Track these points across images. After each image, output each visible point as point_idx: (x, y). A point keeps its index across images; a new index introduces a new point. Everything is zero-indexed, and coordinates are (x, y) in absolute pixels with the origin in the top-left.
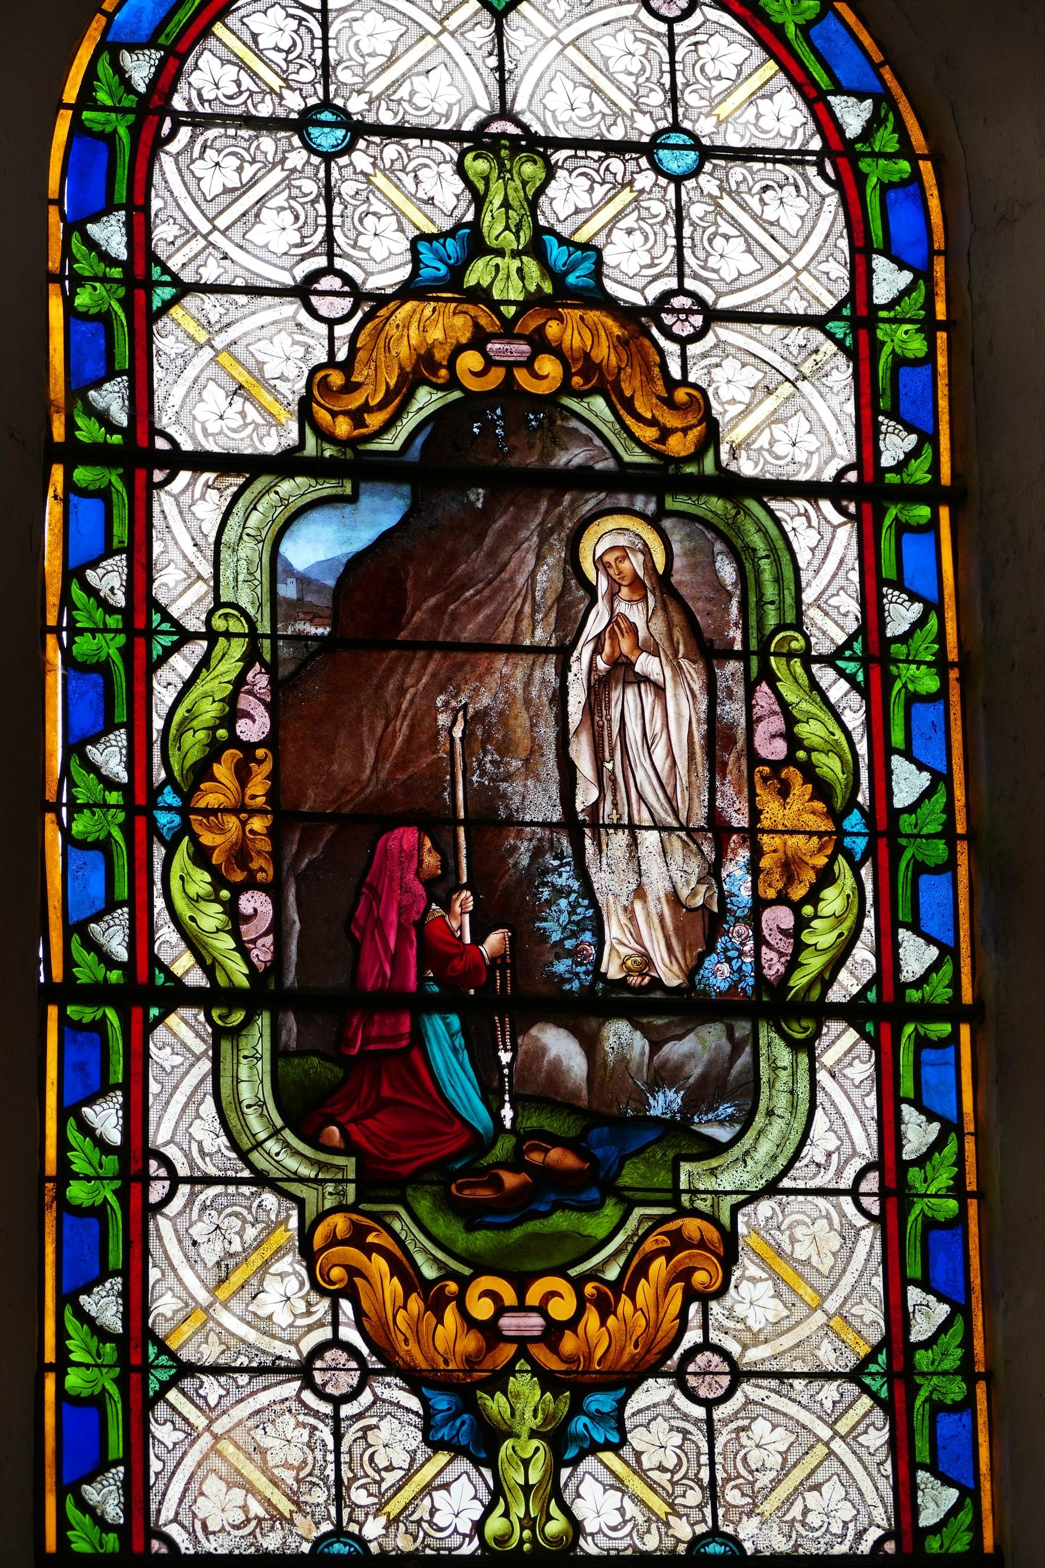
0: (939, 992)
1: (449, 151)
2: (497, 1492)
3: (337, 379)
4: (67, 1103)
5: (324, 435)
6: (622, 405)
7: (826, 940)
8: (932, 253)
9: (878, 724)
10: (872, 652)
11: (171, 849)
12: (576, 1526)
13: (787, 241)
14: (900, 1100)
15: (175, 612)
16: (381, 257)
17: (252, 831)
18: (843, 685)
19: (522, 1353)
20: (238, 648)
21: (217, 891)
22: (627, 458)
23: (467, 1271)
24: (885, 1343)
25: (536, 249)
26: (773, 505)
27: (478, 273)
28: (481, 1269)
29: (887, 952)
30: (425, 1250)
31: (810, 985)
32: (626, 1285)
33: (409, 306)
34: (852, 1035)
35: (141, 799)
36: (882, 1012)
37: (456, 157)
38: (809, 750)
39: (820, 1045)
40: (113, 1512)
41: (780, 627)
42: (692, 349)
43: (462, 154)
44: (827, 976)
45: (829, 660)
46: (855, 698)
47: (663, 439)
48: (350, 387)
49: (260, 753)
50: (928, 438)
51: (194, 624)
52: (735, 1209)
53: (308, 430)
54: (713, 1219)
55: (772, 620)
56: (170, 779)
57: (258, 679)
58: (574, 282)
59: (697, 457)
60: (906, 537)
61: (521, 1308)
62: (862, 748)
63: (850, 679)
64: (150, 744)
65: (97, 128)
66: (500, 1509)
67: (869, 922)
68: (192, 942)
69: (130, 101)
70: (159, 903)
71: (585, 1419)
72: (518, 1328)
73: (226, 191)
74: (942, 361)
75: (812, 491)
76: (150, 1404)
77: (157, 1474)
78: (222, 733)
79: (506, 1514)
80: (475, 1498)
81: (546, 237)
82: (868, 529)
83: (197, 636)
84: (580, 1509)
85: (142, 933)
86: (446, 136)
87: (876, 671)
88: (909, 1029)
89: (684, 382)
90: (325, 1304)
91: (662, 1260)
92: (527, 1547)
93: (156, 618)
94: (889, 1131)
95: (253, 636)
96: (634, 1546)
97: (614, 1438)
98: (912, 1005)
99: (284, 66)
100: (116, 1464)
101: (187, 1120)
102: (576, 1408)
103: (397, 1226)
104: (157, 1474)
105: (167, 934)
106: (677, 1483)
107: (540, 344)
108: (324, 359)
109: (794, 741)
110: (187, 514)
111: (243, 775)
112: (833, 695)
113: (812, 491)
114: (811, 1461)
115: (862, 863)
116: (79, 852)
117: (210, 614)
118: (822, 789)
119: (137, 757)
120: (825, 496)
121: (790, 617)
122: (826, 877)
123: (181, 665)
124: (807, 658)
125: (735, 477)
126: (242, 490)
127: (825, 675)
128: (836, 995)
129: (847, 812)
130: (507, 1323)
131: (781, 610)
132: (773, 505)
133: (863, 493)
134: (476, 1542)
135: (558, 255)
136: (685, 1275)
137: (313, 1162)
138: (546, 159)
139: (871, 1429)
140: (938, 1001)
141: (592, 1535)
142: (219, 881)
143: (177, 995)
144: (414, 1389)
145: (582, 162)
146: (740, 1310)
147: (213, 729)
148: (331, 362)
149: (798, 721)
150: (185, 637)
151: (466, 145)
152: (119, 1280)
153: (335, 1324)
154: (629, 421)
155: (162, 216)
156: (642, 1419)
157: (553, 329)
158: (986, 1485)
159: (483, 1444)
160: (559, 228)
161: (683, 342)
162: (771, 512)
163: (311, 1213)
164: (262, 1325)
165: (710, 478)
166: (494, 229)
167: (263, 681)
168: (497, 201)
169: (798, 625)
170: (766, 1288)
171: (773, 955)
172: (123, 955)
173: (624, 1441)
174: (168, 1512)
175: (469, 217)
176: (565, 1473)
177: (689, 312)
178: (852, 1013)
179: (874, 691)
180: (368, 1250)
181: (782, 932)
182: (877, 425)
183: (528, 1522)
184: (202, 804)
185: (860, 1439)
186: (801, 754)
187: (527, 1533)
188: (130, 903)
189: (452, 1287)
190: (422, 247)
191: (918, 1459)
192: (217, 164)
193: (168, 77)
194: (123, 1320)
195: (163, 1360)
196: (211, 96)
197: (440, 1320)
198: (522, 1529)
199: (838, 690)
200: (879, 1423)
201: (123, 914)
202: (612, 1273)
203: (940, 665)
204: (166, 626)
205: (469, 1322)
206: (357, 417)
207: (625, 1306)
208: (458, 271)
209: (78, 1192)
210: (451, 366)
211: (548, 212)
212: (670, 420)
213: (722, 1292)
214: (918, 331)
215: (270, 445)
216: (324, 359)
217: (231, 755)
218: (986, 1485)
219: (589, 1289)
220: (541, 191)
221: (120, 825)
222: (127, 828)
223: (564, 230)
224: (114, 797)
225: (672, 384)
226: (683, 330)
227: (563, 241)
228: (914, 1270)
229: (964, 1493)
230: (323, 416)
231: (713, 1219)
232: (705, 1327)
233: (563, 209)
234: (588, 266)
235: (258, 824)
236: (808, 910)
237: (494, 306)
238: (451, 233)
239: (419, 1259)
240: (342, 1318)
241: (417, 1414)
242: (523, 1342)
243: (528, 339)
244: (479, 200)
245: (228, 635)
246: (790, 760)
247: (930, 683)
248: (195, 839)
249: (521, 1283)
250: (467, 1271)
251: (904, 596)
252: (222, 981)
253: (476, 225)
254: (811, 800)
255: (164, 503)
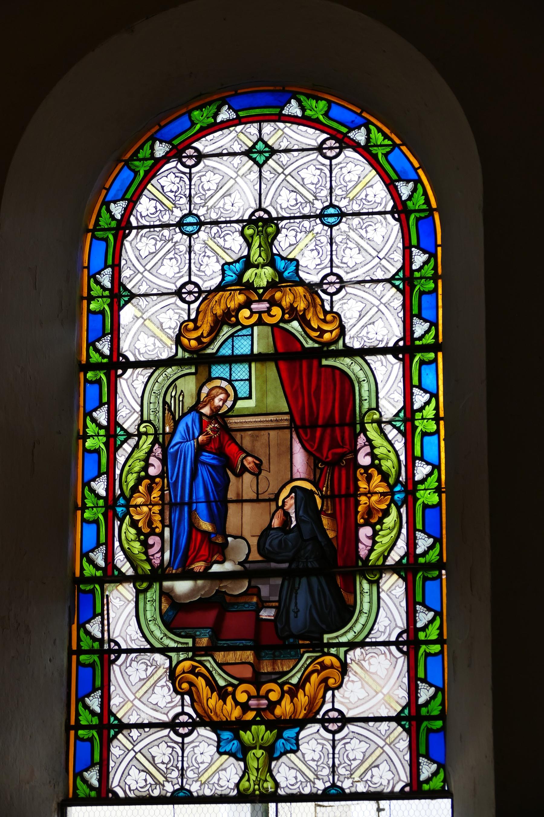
0: (429, 340)
1: (238, 227)
2: (246, 771)
3: (191, 325)
4: (77, 771)
5: (185, 349)
6: (305, 322)
7: (386, 540)
8: (437, 246)
9: (414, 746)
10: (409, 413)
11: (122, 521)
12: (277, 785)
13: (375, 244)
14: (416, 530)
15: (125, 426)
16: (210, 276)
17: (153, 513)
18: (395, 432)
19: (260, 296)
20: (151, 438)
21: (139, 537)
22: (306, 346)
23: (236, 682)
24: (408, 705)
25: (272, 263)
26: (367, 358)
27: (249, 275)
28: (242, 681)
29: (412, 543)
30: (220, 675)
31: (378, 559)
32: (301, 685)
33: (221, 293)
34: (395, 577)
35: (110, 503)
36: (408, 569)
37: (240, 229)
38: (380, 460)
39: (382, 582)
40: (95, 782)
41: (370, 409)
42: (335, 298)
43: (243, 228)
44: (386, 554)
45: (389, 422)
46: (400, 437)
47: (321, 336)
48: (196, 328)
49: (157, 480)
50: (433, 255)
51: (132, 430)
52: (346, 653)
53: (179, 348)
54: (337, 656)
55: (366, 406)
56: (122, 494)
57: (158, 450)
58: (287, 277)
59: (335, 341)
60: (427, 511)
61: (260, 313)
62: (402, 458)
63: (398, 429)
64: (115, 480)
65: (87, 662)
66: (246, 778)
67: (404, 531)
68: (129, 557)
69: (114, 224)
70: (117, 544)
71: (283, 741)
72: (257, 308)
73: (150, 253)
74: (440, 291)
75: (384, 351)
76: (110, 740)
77: (112, 767)
78: (143, 474)
79: (248, 780)
80: (236, 774)
81: (275, 257)
82: (405, 224)
83: (135, 435)
84: (278, 778)
85: (109, 557)
86: (237, 222)
87: (409, 424)
88: (420, 574)
89: (331, 312)
90: (179, 697)
91: (315, 675)
92: (257, 792)
93: (118, 429)
94: (414, 769)
95: (156, 434)
96: (300, 792)
97: (295, 748)
98: (422, 564)
99: (174, 198)
100: (108, 334)
101: (125, 626)
102: (279, 736)
103: (208, 665)
104: (112, 767)
105: (120, 556)
106: (317, 188)
107: (273, 302)
108: (186, 318)
109: (374, 456)
110: (131, 387)
111: (150, 490)
112: (390, 437)
113: (384, 351)
114: (374, 686)
115: (401, 506)
116: (83, 668)
117: (139, 425)
118: (385, 476)
119: (110, 488)
120: (389, 353)
121: (374, 405)
122: (386, 513)
123: (127, 447)
124: (379, 422)
125: (352, 349)
126: (152, 374)
127: (388, 428)
128: (390, 562)
129: (395, 485)
130: (252, 702)
131: (370, 403)
132: (367, 358)
133: (405, 350)
134: (236, 792)
135: (281, 264)
136: (325, 680)
137: (175, 642)
138: (277, 225)
139: (401, 741)
140: (433, 561)
141: (283, 788)
142: (139, 532)
143: (122, 579)
144: (214, 730)
145: (292, 224)
146: (347, 695)
147: (139, 473)
148: (189, 320)
149: (375, 448)
150: (129, 436)
151: (245, 224)
152: (105, 476)
153: (183, 705)
154: (307, 330)
155: (125, 267)
156: (304, 740)
157: (278, 295)
158: (444, 536)
159: (242, 753)
160: (282, 253)
161: (332, 295)
162: (366, 361)
163: (174, 663)
164: (154, 707)
165: (341, 350)
166: (255, 257)
167: (159, 451)
168: (257, 244)
169: (377, 408)
170: (358, 684)
171: (364, 546)
172: (98, 710)
173: (298, 749)
174: (115, 783)
175: (246, 253)
176: (274, 763)
177: (334, 283)
178: (396, 569)
179: (408, 433)
180: (197, 675)
181: (368, 537)
182: (417, 686)
183: (258, 782)
184: (134, 503)
185: (396, 745)
186: (377, 462)
187: (257, 787)
188: (106, 544)
189: (230, 689)
190: (226, 267)
191: (413, 244)
192: (148, 210)
193: (128, 211)
194: (110, 350)
195: (122, 433)
196: (135, 638)
197: (225, 703)
198: (255, 785)
199: (392, 433)
200: (405, 738)
201: (104, 477)
202: (295, 681)
203: (437, 419)
204: (122, 433)
205: (237, 703)
206: (198, 339)
207: (301, 694)
208: (241, 275)
209: (90, 443)
210: (237, 317)
211: (278, 247)
212: (325, 327)
213: (340, 686)
214: (434, 492)
215: (164, 356)
216: (186, 318)
217: (146, 482)
218: (444, 536)
219: (286, 688)
220: (275, 238)
221: (108, 305)
222: (105, 515)
223: (284, 254)
224: (102, 432)
225: (326, 313)
226: (332, 290)
227: (283, 258)
228: (423, 750)
229: (438, 689)
230: (185, 341)
231: (337, 656)
232: (333, 702)
233: (284, 245)
234: (292, 268)
235: (156, 509)
236: (378, 527)
237: (255, 290)
238: (237, 261)
239: (217, 678)
240: (185, 703)
241: (215, 741)
242: (260, 301)
243: (268, 301)
244: (249, 246)
245: (146, 434)
246: (372, 465)
247: (432, 427)
248: (131, 517)
249: (258, 686)
250: (236, 682)
251: (423, 463)
252: (140, 571)
253: (248, 257)
254: (380, 482)
255: (122, 384)
